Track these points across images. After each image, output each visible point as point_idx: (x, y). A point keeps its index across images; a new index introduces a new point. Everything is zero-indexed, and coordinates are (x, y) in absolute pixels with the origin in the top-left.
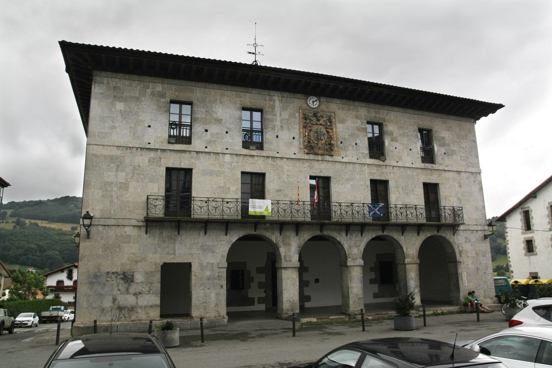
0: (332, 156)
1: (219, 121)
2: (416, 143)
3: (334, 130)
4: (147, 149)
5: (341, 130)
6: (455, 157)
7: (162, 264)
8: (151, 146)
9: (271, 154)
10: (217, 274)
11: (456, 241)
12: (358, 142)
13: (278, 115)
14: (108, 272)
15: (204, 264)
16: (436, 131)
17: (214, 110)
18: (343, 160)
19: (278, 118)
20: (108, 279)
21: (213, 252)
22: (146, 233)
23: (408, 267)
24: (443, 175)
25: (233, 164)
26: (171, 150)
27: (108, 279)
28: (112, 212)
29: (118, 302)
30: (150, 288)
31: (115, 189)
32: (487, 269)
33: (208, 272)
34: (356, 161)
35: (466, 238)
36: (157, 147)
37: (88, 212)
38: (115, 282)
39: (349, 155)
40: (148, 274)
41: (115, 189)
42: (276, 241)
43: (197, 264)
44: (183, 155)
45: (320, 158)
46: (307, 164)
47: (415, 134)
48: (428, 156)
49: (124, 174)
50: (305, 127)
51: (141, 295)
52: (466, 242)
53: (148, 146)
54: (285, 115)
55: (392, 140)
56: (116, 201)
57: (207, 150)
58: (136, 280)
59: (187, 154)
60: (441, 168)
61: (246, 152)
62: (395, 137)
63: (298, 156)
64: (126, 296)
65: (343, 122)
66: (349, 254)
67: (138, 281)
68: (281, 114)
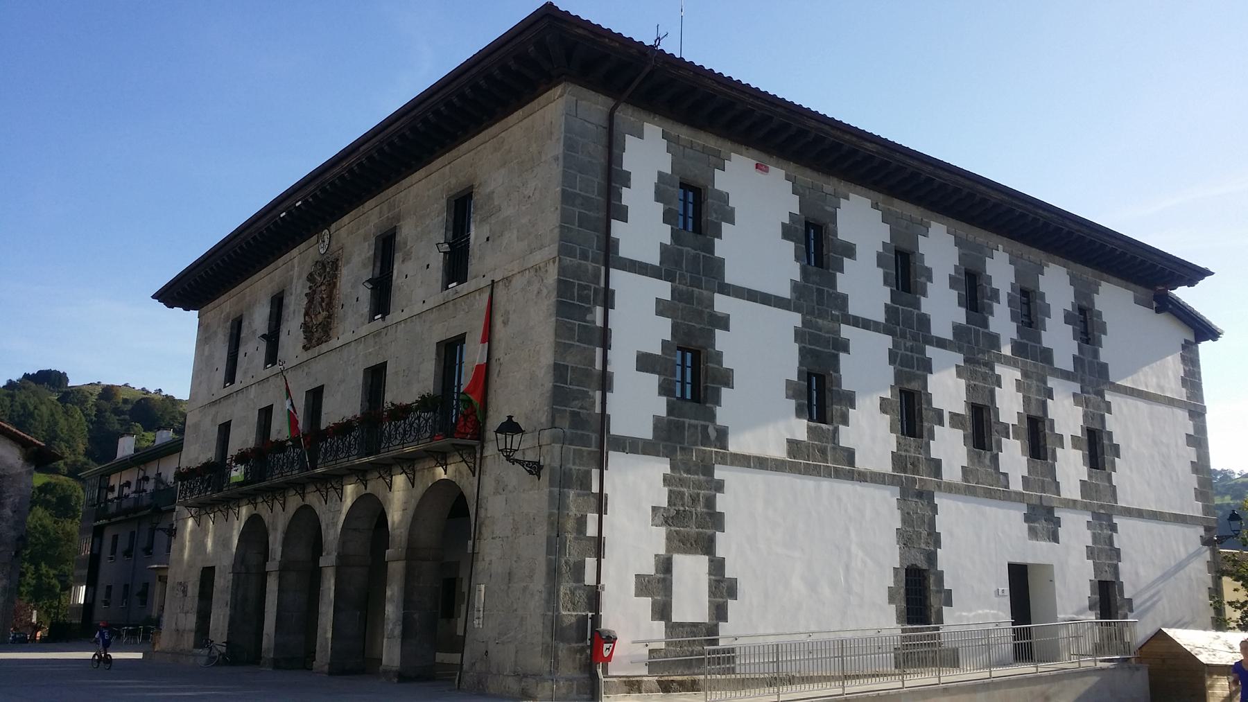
52: (496, 493)
61: (310, 354)
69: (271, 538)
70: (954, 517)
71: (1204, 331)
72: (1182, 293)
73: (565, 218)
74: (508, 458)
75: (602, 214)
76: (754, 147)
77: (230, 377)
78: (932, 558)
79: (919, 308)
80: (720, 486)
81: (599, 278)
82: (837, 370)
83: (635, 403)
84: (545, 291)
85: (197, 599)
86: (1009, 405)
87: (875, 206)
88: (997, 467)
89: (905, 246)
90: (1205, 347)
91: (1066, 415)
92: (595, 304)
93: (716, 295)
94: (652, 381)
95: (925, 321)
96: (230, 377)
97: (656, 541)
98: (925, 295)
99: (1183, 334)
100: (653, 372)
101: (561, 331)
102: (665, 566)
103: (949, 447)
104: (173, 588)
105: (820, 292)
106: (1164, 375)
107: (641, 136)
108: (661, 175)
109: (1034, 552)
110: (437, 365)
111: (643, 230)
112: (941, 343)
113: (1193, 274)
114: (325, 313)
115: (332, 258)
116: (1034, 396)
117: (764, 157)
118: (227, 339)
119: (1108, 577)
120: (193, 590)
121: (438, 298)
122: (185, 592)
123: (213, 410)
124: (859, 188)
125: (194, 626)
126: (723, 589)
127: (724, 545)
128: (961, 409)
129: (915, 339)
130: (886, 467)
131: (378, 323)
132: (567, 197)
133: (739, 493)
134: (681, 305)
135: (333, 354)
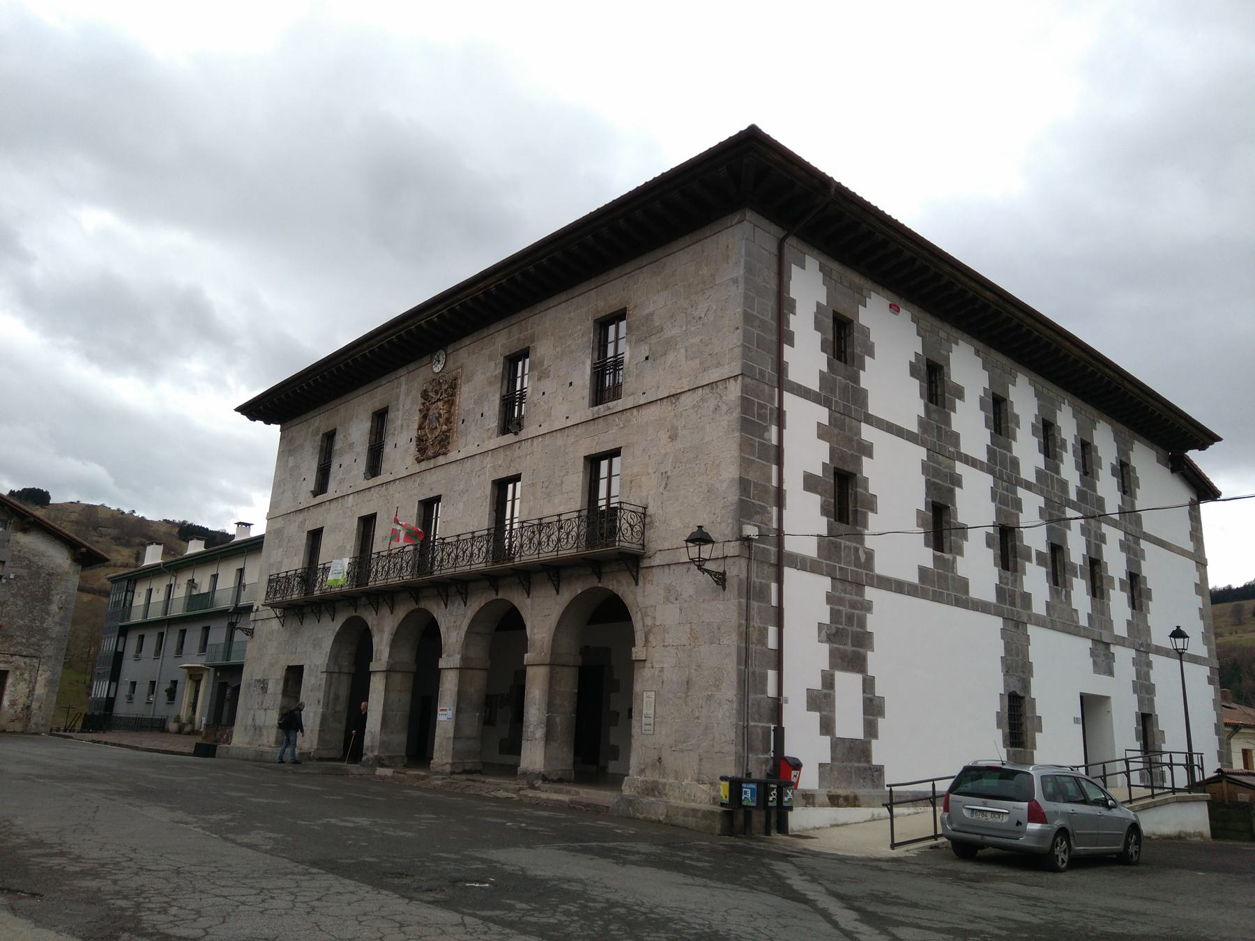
6: (671, 357)
11: (640, 599)
23: (530, 672)
24: (634, 421)
35: (668, 589)
37: (700, 527)
40: (277, 680)
52: (667, 600)
61: (424, 465)
69: (375, 640)
70: (1045, 646)
71: (1205, 491)
72: (1193, 455)
73: (747, 337)
74: (700, 567)
75: (774, 338)
76: (889, 289)
77: (321, 487)
78: (1026, 685)
79: (1011, 451)
80: (868, 607)
81: (773, 399)
82: (954, 505)
83: (805, 521)
84: (724, 408)
85: (280, 697)
86: (1076, 549)
87: (977, 353)
88: (1070, 604)
89: (999, 392)
90: (1206, 508)
91: (1116, 564)
92: (771, 423)
93: (863, 424)
94: (815, 500)
95: (1015, 463)
96: (321, 487)
97: (820, 655)
98: (1015, 439)
99: (1184, 494)
100: (817, 492)
101: (745, 446)
102: (828, 682)
103: (1035, 580)
104: (250, 685)
105: (939, 428)
106: (1173, 527)
107: (803, 267)
108: (818, 304)
109: (1098, 685)
110: (585, 476)
111: (806, 359)
112: (1028, 486)
113: (1205, 438)
114: (444, 427)
115: (449, 378)
116: (1092, 540)
117: (897, 301)
118: (317, 450)
119: (1146, 711)
120: (275, 687)
121: (589, 413)
122: (264, 689)
123: (301, 517)
124: (965, 335)
125: (276, 722)
126: (873, 708)
127: (874, 662)
128: (1044, 548)
129: (1009, 481)
130: (991, 597)
131: (510, 438)
132: (748, 318)
133: (887, 615)
134: (836, 431)
135: (454, 465)
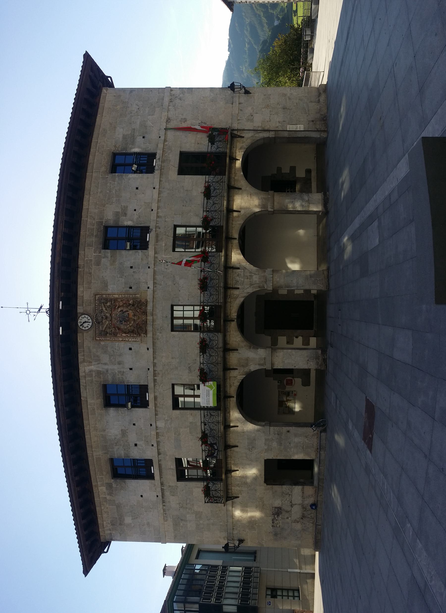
0: (147, 302)
1: (124, 433)
2: (129, 179)
3: (117, 296)
4: (163, 497)
5: (115, 286)
6: (149, 123)
7: (265, 485)
8: (160, 495)
9: (151, 378)
10: (276, 436)
12: (128, 264)
13: (106, 367)
14: (272, 526)
15: (266, 447)
16: (115, 146)
17: (113, 437)
18: (151, 287)
19: (110, 367)
20: (278, 526)
21: (255, 439)
22: (238, 497)
25: (166, 418)
26: (161, 478)
27: (278, 526)
28: (221, 523)
29: (298, 518)
30: (287, 494)
31: (201, 522)
32: (285, 95)
33: (273, 444)
34: (151, 270)
36: (159, 489)
38: (280, 521)
39: (145, 278)
41: (201, 522)
42: (244, 375)
43: (266, 454)
44: (163, 466)
45: (150, 318)
46: (158, 334)
47: (117, 179)
48: (145, 163)
49: (188, 516)
50: (115, 335)
51: (293, 502)
53: (160, 497)
54: (105, 358)
55: (125, 215)
56: (212, 521)
57: (155, 445)
58: (280, 506)
59: (162, 463)
60: (161, 146)
62: (122, 209)
63: (150, 345)
64: (293, 512)
65: (105, 285)
66: (259, 287)
67: (281, 504)
68: (105, 364)
